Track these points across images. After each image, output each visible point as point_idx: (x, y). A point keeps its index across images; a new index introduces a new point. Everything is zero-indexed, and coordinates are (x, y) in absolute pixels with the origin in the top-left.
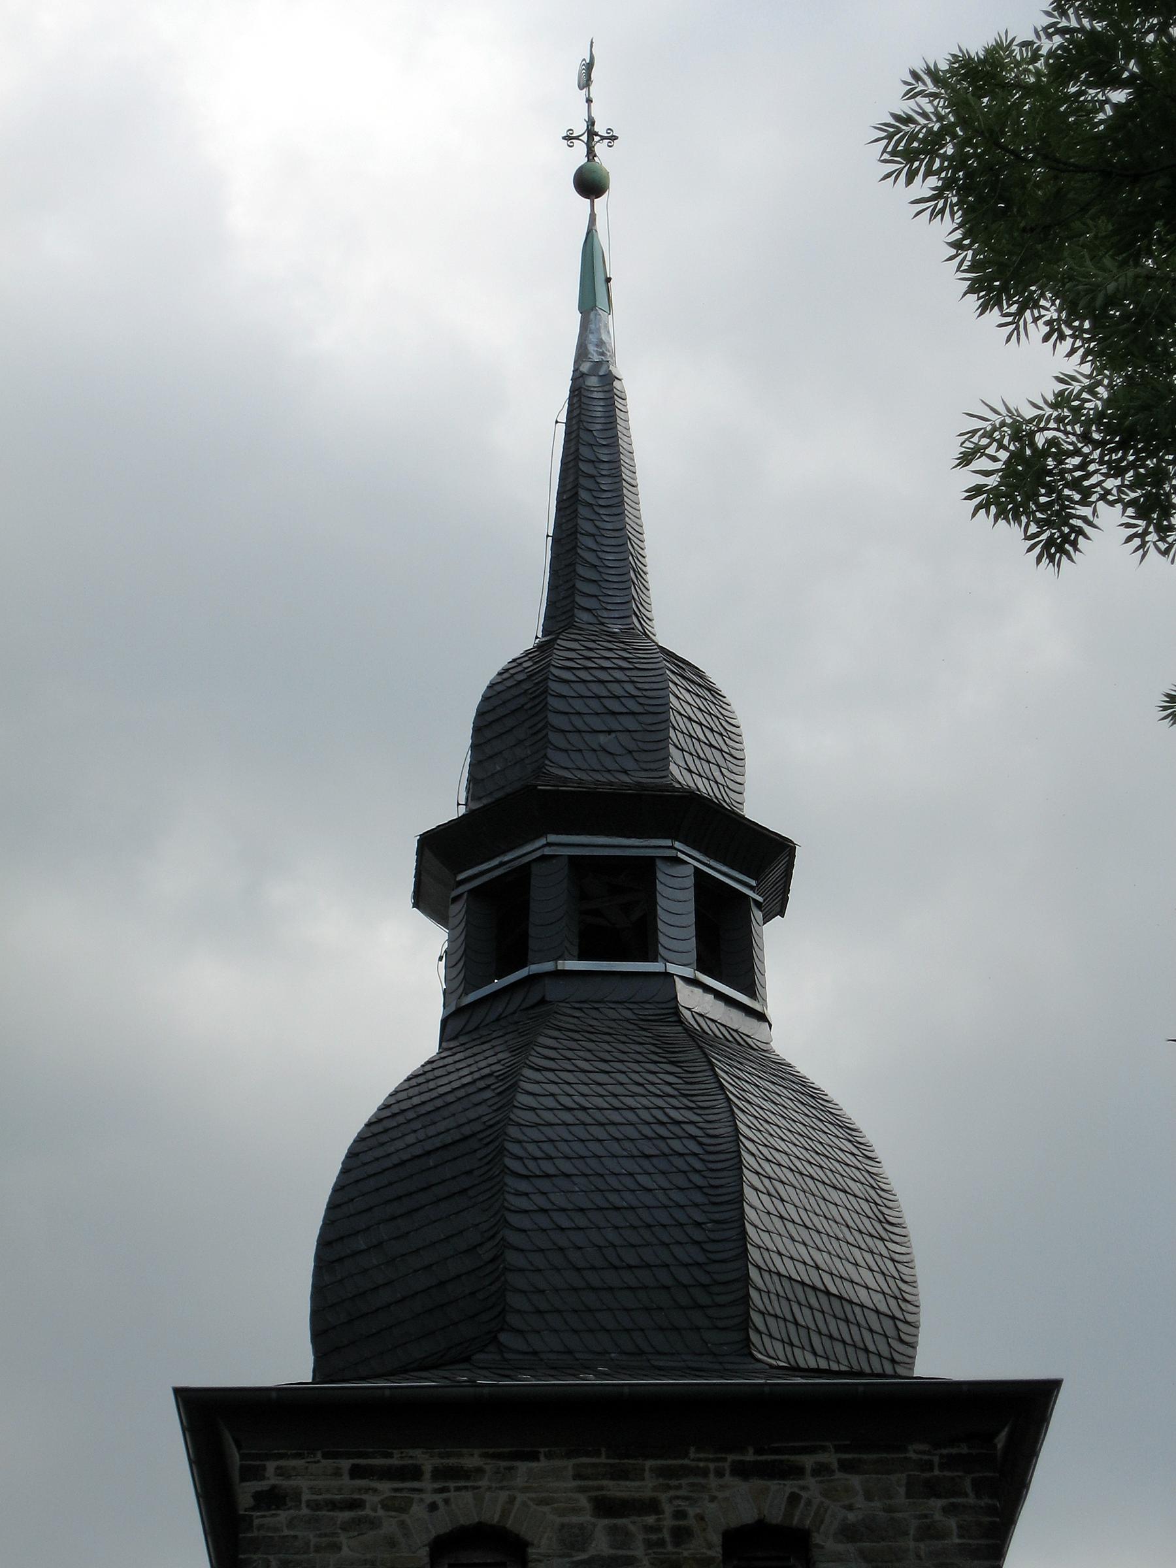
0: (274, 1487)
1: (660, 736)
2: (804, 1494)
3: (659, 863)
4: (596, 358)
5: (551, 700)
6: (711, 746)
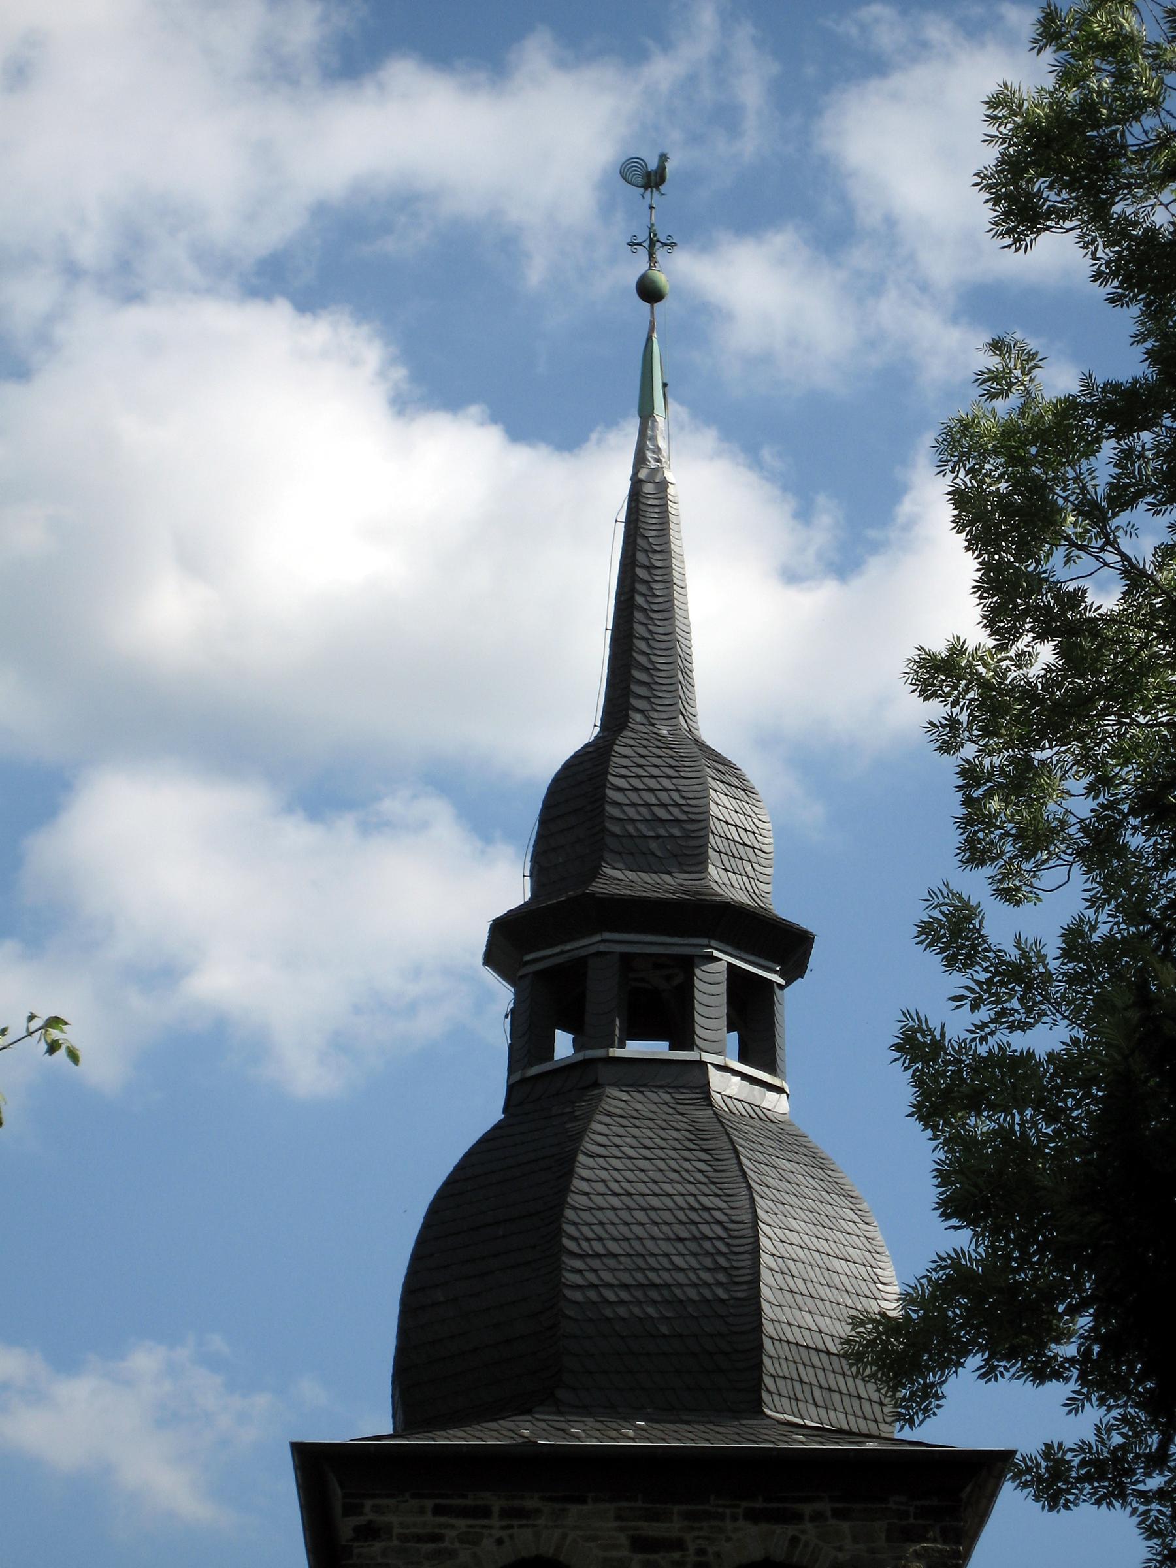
0: (370, 1522)
1: (701, 825)
2: (803, 1538)
3: (697, 960)
4: (653, 464)
5: (608, 808)
6: (745, 844)
